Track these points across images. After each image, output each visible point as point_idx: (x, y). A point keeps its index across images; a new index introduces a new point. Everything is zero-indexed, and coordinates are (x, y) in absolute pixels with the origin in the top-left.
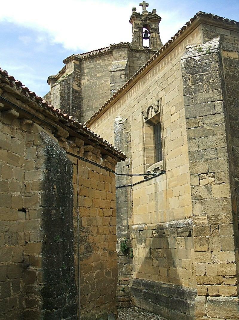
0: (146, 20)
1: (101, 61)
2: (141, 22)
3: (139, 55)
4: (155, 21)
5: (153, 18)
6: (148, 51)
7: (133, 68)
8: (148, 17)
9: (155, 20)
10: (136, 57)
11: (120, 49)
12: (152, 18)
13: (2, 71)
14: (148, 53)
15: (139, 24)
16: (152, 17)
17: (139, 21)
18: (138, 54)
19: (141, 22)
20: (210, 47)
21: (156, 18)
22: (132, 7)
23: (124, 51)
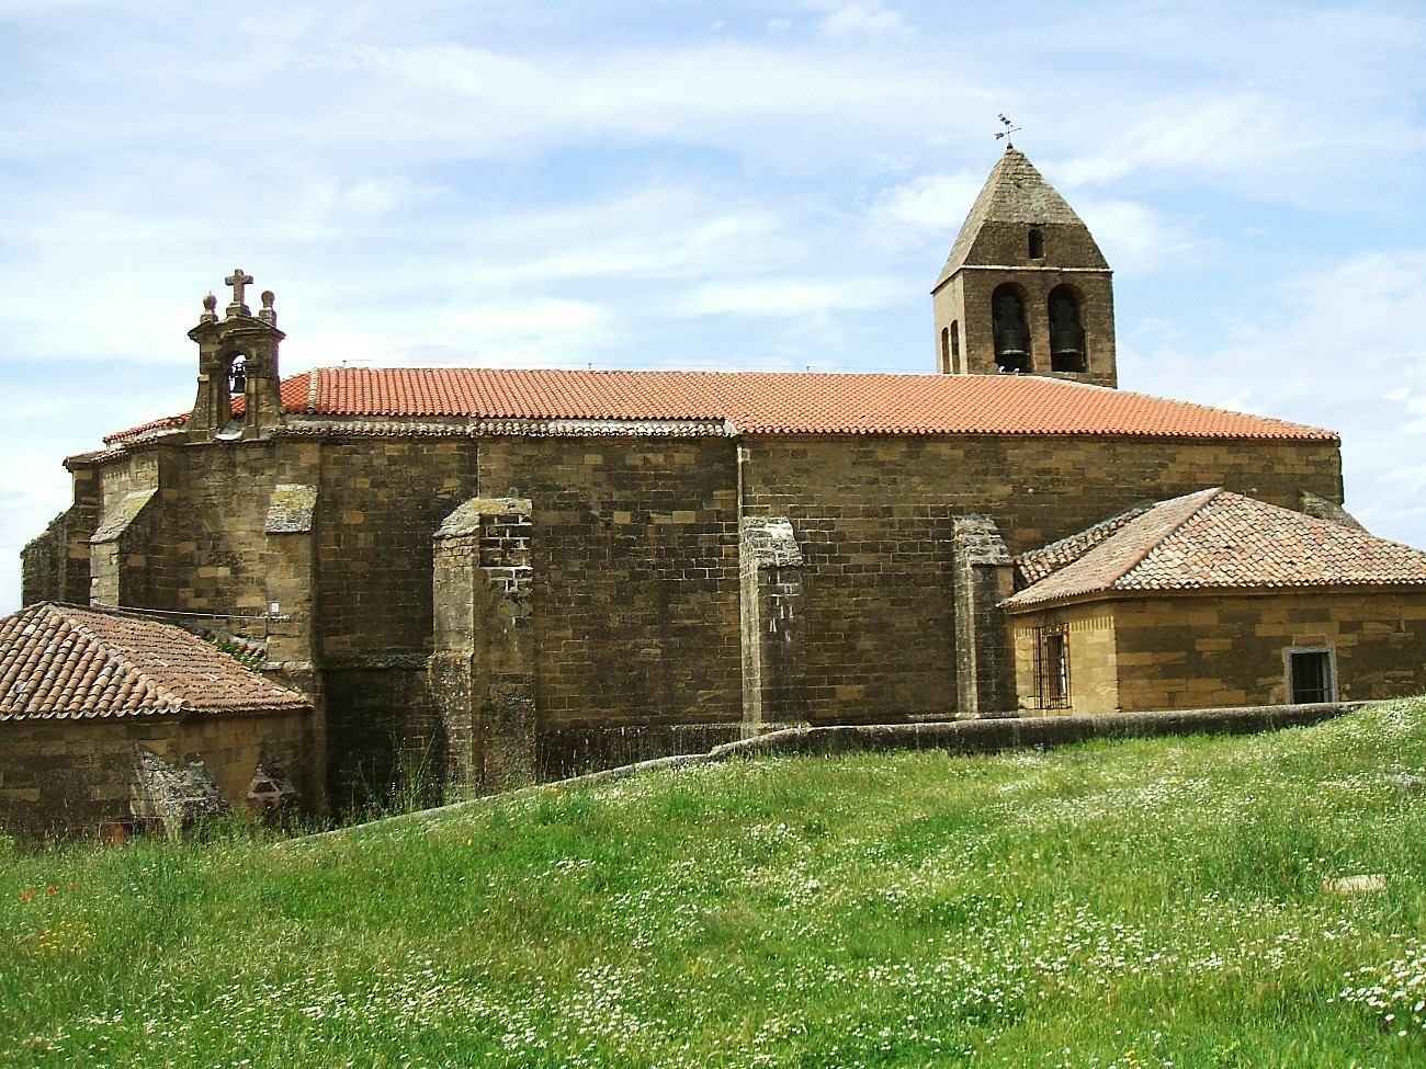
19: (219, 347)
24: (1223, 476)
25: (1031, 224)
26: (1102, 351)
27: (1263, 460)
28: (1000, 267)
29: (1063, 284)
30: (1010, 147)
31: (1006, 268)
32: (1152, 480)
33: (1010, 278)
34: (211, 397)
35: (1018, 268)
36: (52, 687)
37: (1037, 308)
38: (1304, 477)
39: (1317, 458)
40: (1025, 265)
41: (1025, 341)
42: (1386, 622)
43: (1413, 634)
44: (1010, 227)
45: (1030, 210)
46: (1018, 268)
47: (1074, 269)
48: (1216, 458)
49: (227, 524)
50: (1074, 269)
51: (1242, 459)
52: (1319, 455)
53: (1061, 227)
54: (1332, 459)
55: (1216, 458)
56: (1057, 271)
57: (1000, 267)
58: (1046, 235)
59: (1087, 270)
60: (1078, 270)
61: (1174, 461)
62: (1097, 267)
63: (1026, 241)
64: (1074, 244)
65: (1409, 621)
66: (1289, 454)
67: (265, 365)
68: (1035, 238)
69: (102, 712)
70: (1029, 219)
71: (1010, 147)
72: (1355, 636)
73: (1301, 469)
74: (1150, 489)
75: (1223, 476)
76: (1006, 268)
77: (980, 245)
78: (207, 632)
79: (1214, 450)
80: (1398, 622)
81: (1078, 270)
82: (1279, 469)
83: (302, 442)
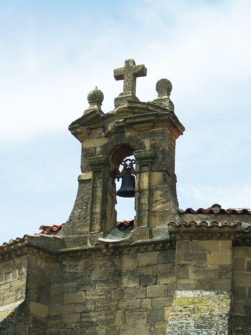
0: (120, 130)
1: (238, 247)
2: (105, 141)
3: (85, 269)
4: (153, 127)
5: (141, 120)
6: (111, 248)
7: (58, 321)
8: (124, 121)
9: (151, 124)
10: (74, 277)
11: (11, 262)
12: (137, 120)
13: (117, 179)
14: (113, 254)
15: (98, 149)
16: (135, 118)
17: (100, 137)
18: (80, 266)
19: (105, 141)
20: (5, 288)
21: (150, 118)
22: (90, 89)
23: (20, 268)
34: (92, 213)
67: (161, 156)
83: (209, 238)
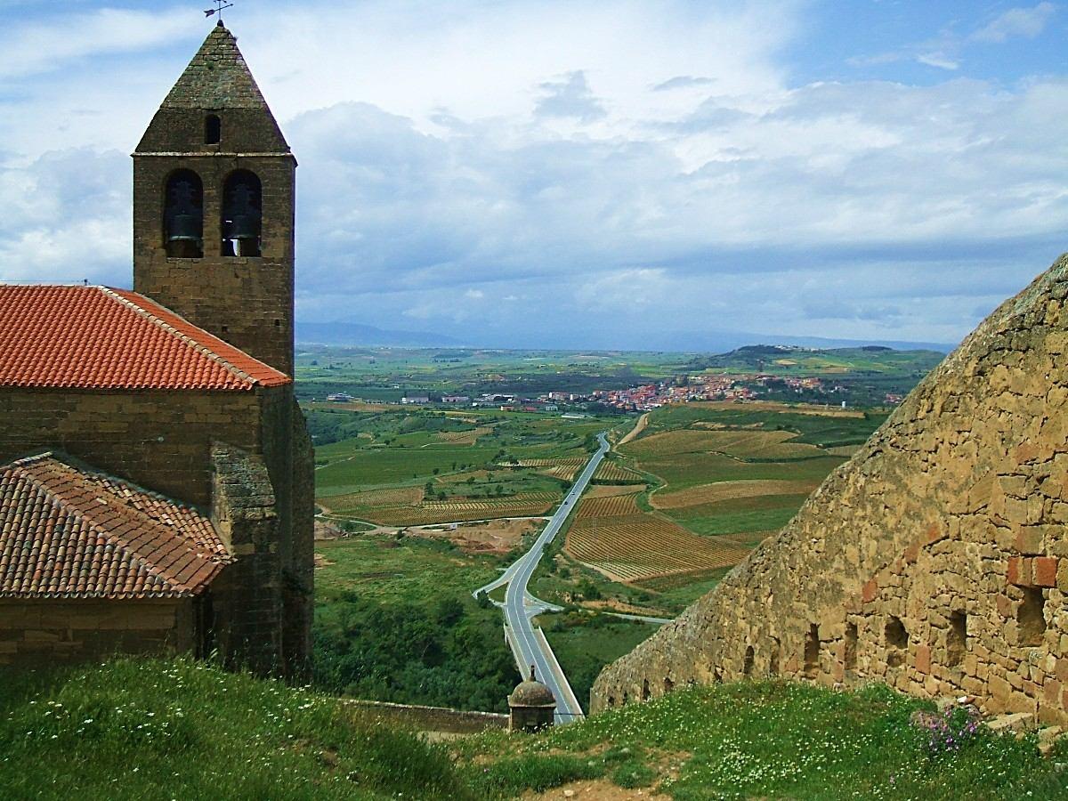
24: (127, 425)
25: (209, 110)
26: (275, 235)
27: (172, 409)
28: (171, 154)
29: (238, 169)
30: (220, 24)
31: (178, 154)
32: (49, 428)
33: (183, 164)
35: (190, 154)
36: (22, 520)
37: (209, 194)
38: (217, 426)
39: (234, 407)
40: (198, 151)
41: (196, 227)
42: (51, 631)
43: (81, 643)
44: (186, 113)
45: (220, 92)
46: (190, 154)
47: (250, 155)
48: (120, 408)
49: (1035, 76)
50: (250, 155)
51: (149, 408)
52: (237, 402)
53: (239, 111)
54: (252, 408)
55: (120, 408)
56: (231, 156)
57: (171, 154)
58: (224, 120)
59: (264, 154)
60: (254, 155)
61: (73, 409)
62: (276, 151)
63: (202, 127)
64: (252, 128)
65: (78, 630)
66: (202, 403)
68: (213, 126)
69: (91, 595)
70: (208, 103)
71: (220, 24)
72: (14, 644)
73: (212, 419)
74: (47, 437)
75: (127, 425)
76: (178, 154)
77: (153, 132)
78: (800, 368)
79: (119, 399)
80: (65, 631)
81: (254, 155)
82: (188, 417)
